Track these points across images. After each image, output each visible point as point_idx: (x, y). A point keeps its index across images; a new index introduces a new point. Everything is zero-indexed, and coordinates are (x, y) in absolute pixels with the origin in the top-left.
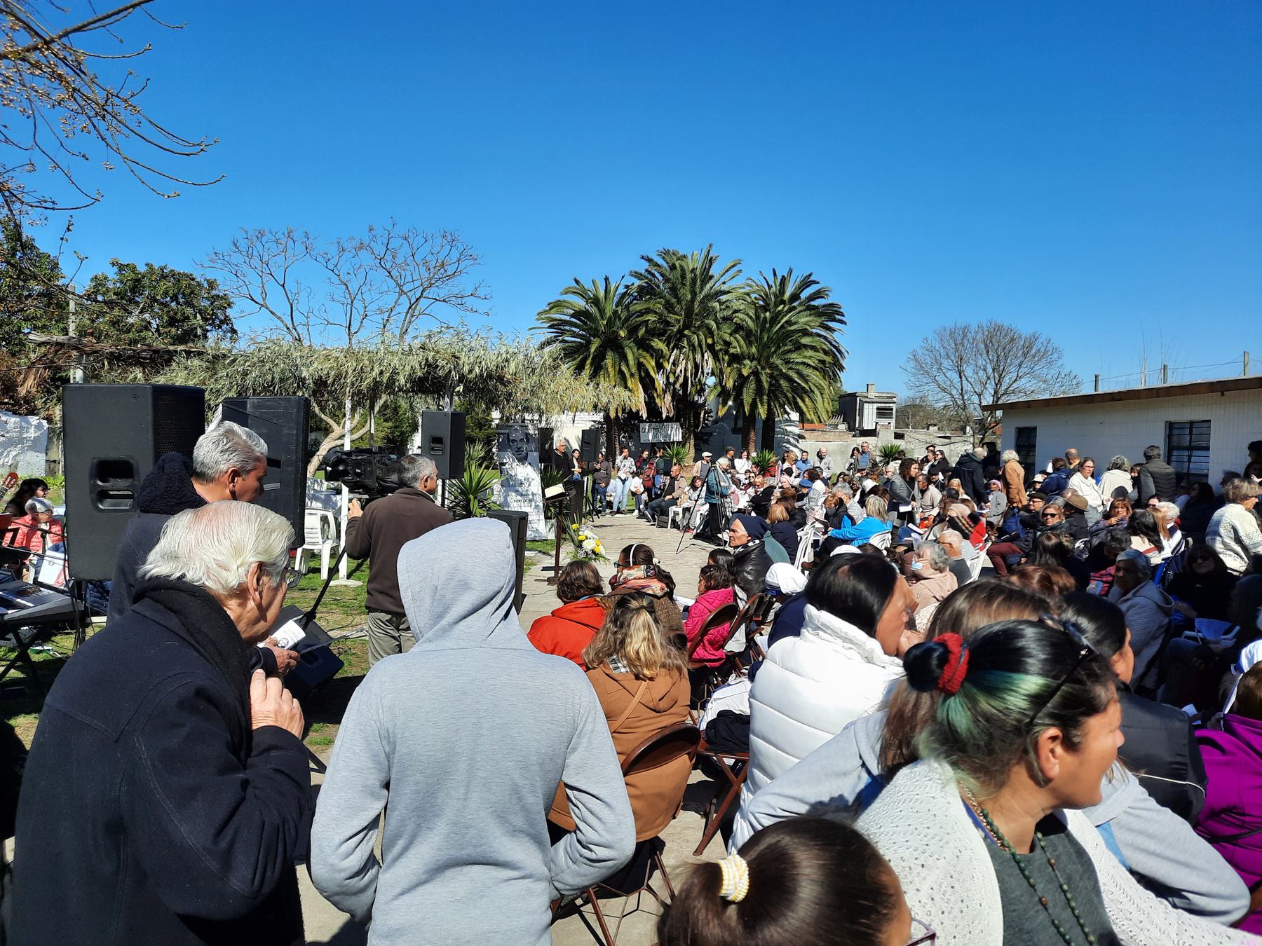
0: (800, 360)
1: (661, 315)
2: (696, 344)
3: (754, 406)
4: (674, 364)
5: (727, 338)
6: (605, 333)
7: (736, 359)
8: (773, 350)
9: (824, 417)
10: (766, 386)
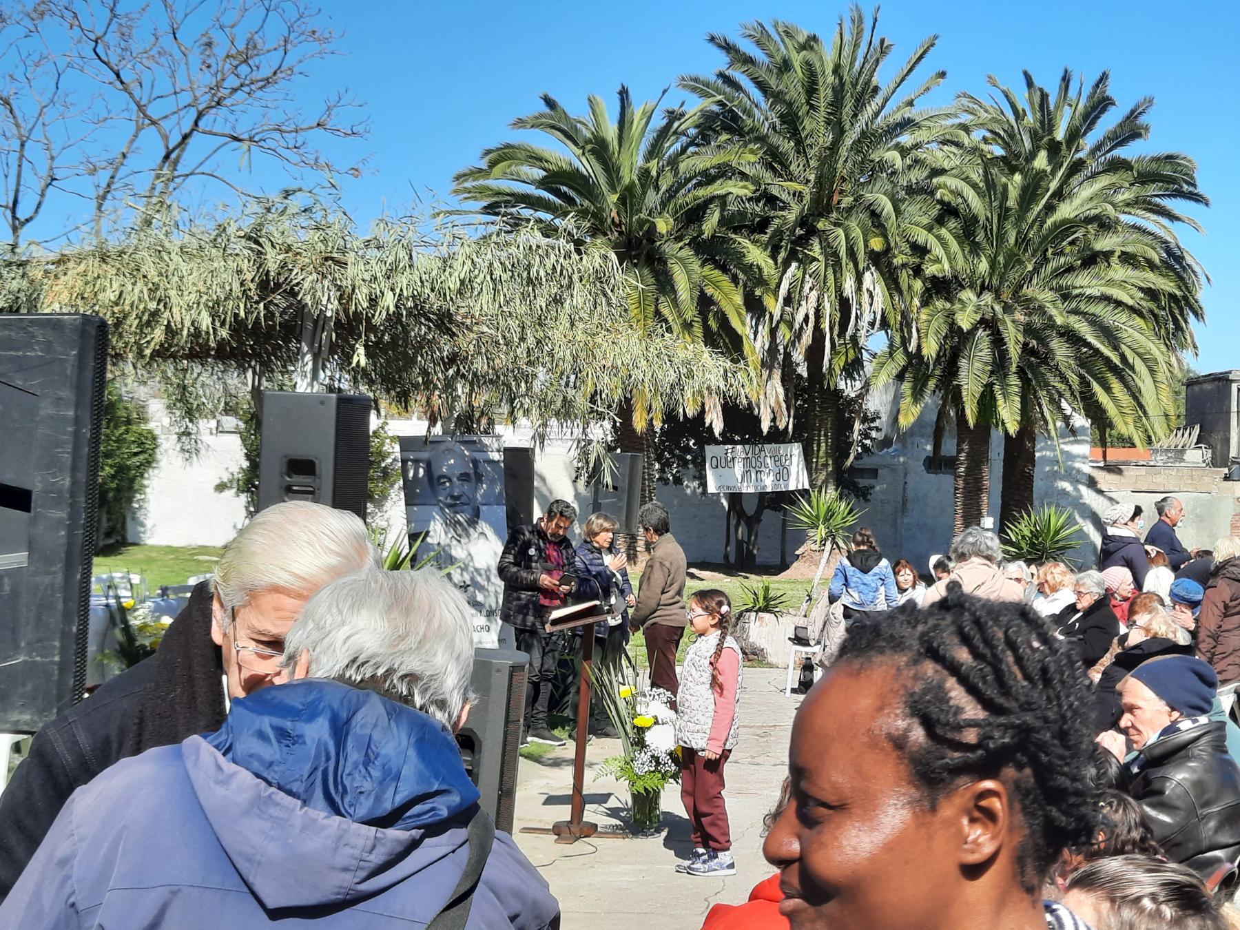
0: (1095, 292)
1: (756, 181)
2: (843, 252)
3: (987, 402)
4: (788, 301)
5: (922, 236)
6: (620, 225)
7: (941, 288)
8: (1030, 268)
9: (1159, 427)
10: (1014, 351)
